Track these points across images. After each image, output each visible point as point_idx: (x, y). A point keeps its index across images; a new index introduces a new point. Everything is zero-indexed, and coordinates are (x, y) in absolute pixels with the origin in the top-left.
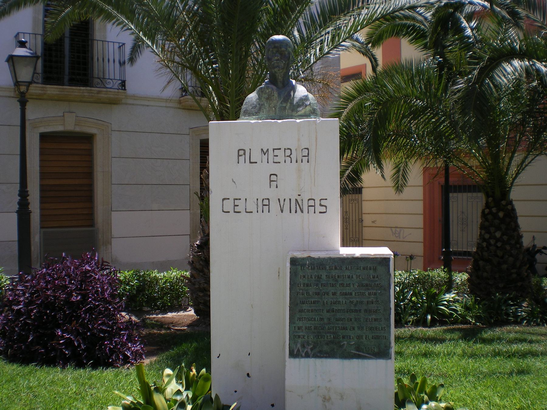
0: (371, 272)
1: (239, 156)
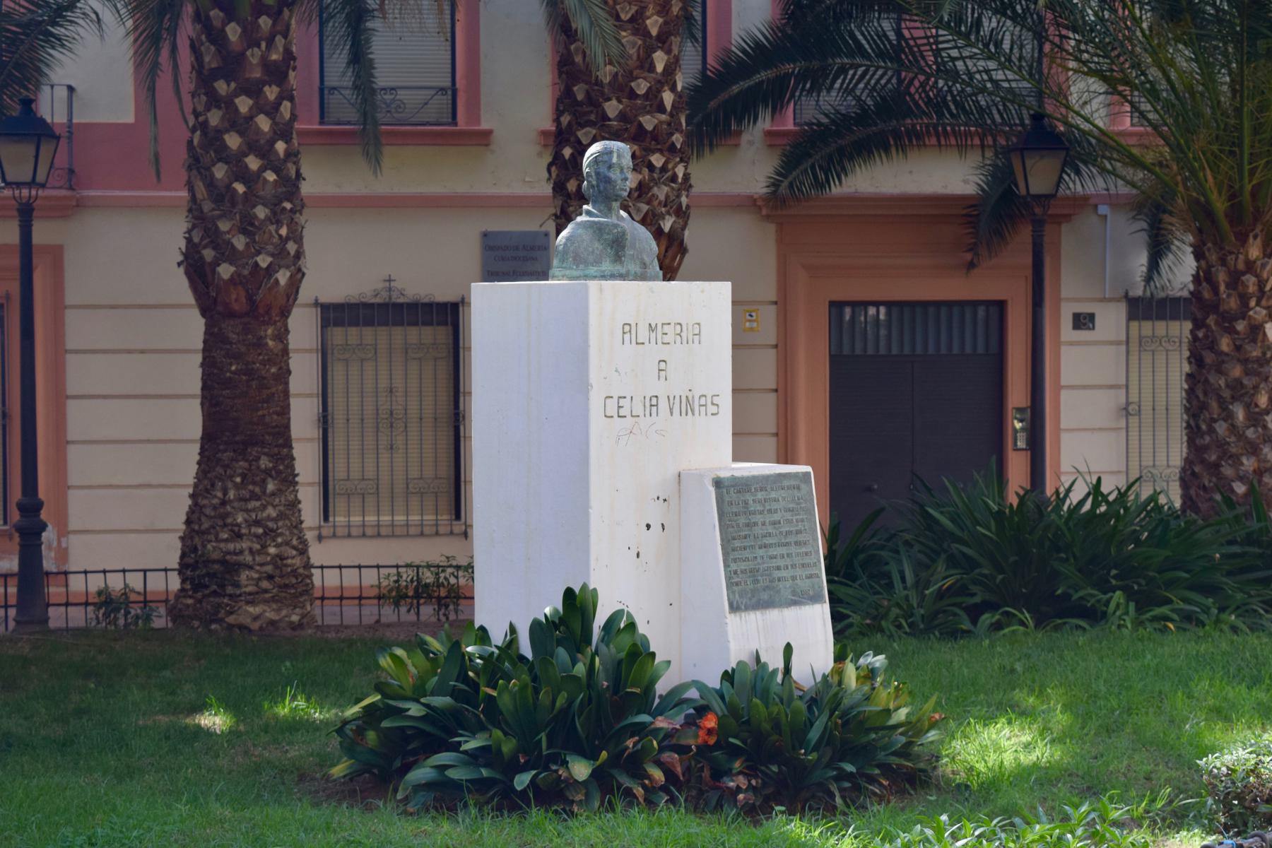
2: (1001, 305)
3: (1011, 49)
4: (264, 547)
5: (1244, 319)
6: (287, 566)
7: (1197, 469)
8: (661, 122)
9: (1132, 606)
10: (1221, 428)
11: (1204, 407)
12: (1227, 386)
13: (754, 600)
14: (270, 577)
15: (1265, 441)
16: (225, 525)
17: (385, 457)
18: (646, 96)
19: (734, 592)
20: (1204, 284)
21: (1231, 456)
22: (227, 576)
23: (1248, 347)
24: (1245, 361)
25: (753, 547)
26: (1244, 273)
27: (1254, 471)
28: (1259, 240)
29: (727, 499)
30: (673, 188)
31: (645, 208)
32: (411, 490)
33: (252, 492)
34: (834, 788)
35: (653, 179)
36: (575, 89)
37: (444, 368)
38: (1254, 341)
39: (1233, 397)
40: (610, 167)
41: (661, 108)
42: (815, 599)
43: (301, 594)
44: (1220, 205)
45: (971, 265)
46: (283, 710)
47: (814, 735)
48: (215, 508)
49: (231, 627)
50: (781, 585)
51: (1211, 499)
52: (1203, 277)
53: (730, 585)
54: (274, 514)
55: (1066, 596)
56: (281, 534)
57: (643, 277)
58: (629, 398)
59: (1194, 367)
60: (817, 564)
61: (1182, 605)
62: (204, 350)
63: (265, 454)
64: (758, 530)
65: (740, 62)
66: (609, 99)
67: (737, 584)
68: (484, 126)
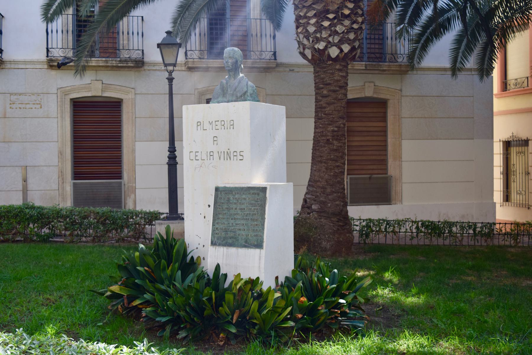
0: (256, 196)
1: (198, 126)
13: (224, 242)
19: (214, 237)
29: (220, 196)
58: (200, 152)
64: (232, 212)
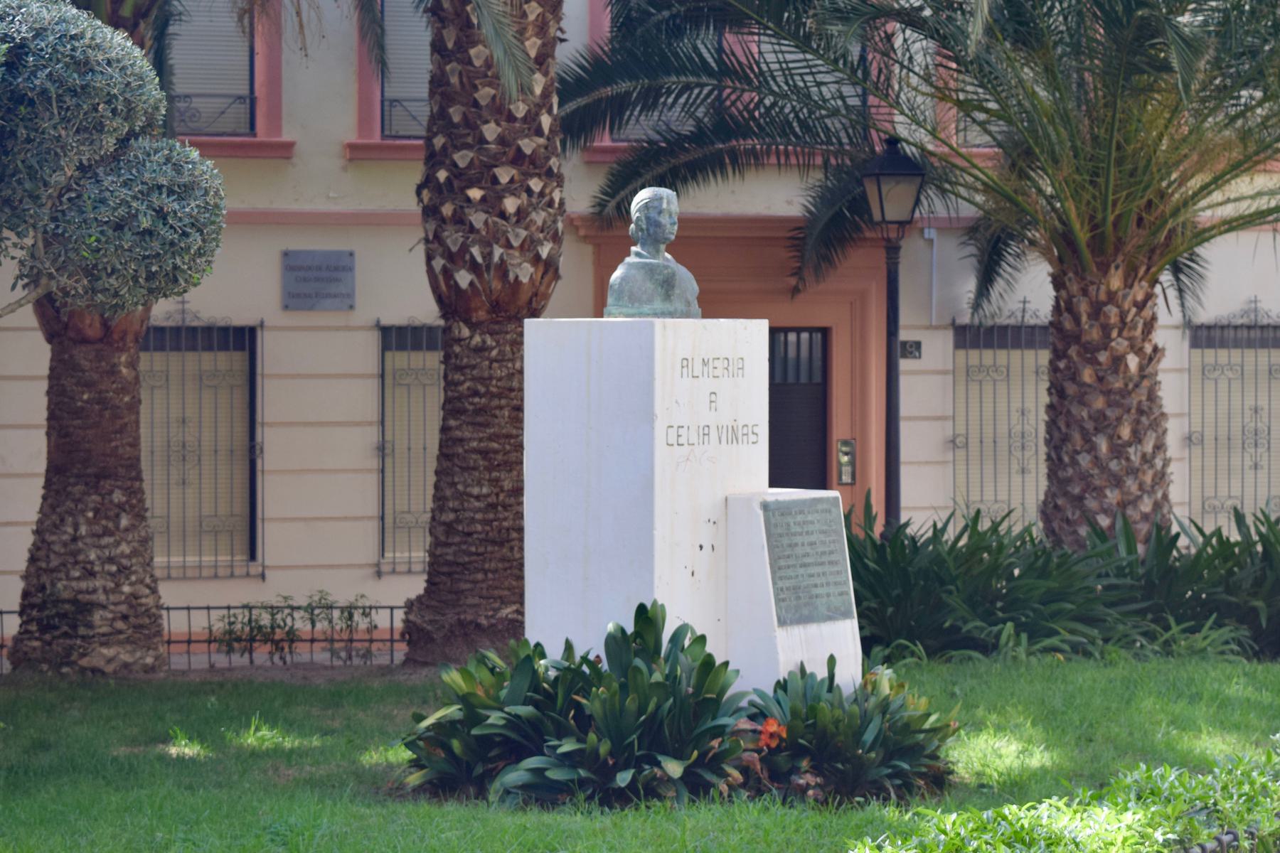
2: (825, 332)
3: (879, 77)
4: (118, 585)
5: (1105, 349)
6: (141, 605)
7: (1060, 502)
8: (539, 146)
9: (1024, 636)
10: (1084, 460)
11: (1066, 439)
12: (1090, 417)
14: (125, 618)
15: (1128, 474)
16: (76, 563)
17: (175, 493)
18: (525, 119)
20: (1066, 315)
21: (1095, 489)
22: (80, 617)
23: (1110, 378)
24: (1107, 393)
25: (794, 566)
26: (1105, 304)
27: (1118, 504)
28: (1120, 271)
29: (773, 521)
30: (549, 214)
31: (523, 233)
32: (205, 528)
33: (105, 528)
34: (888, 784)
35: (530, 204)
36: (451, 110)
37: (241, 397)
38: (1116, 372)
39: (1096, 429)
40: (660, 212)
41: (539, 132)
42: (846, 615)
43: (155, 636)
44: (1082, 235)
45: (795, 291)
46: (250, 739)
47: (869, 736)
48: (65, 544)
49: (83, 670)
50: (818, 601)
51: (1075, 532)
52: (1063, 307)
53: (778, 601)
54: (128, 551)
55: (955, 629)
56: (135, 572)
57: (687, 315)
59: (1055, 399)
60: (846, 583)
61: (1068, 636)
62: (50, 377)
63: (119, 487)
64: (799, 551)
65: (579, 79)
66: (487, 122)
67: (784, 600)
68: (286, 137)
